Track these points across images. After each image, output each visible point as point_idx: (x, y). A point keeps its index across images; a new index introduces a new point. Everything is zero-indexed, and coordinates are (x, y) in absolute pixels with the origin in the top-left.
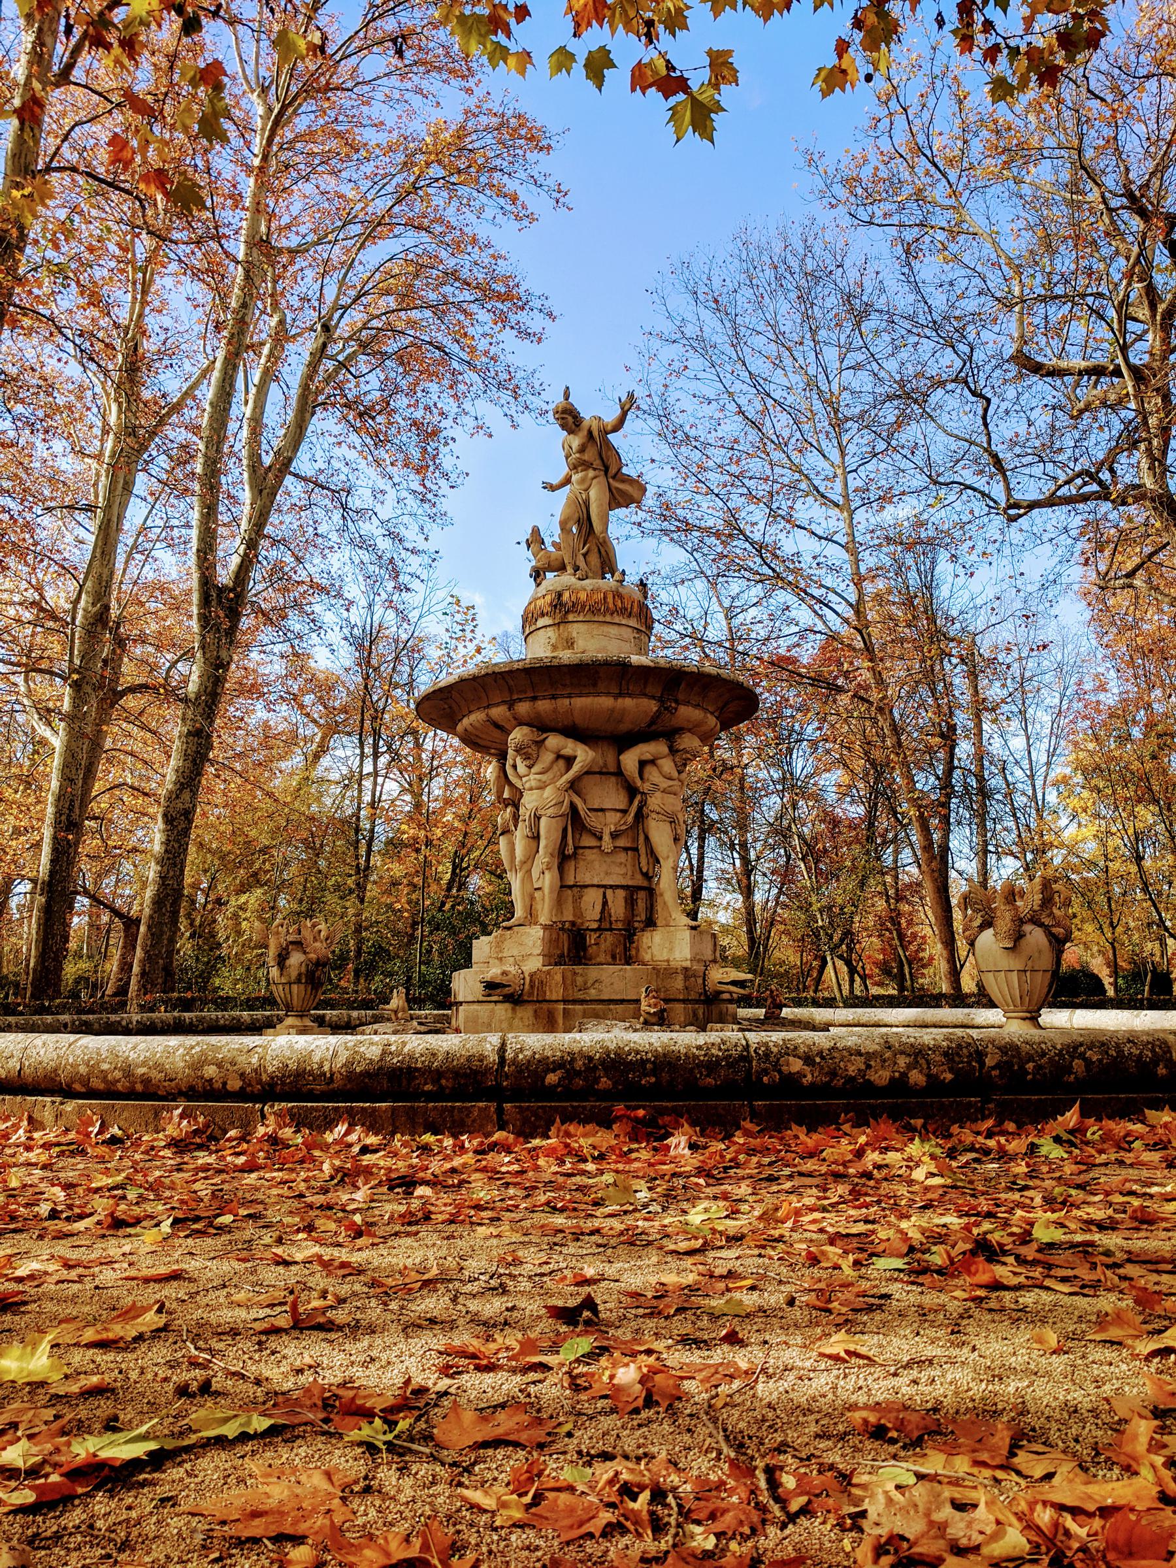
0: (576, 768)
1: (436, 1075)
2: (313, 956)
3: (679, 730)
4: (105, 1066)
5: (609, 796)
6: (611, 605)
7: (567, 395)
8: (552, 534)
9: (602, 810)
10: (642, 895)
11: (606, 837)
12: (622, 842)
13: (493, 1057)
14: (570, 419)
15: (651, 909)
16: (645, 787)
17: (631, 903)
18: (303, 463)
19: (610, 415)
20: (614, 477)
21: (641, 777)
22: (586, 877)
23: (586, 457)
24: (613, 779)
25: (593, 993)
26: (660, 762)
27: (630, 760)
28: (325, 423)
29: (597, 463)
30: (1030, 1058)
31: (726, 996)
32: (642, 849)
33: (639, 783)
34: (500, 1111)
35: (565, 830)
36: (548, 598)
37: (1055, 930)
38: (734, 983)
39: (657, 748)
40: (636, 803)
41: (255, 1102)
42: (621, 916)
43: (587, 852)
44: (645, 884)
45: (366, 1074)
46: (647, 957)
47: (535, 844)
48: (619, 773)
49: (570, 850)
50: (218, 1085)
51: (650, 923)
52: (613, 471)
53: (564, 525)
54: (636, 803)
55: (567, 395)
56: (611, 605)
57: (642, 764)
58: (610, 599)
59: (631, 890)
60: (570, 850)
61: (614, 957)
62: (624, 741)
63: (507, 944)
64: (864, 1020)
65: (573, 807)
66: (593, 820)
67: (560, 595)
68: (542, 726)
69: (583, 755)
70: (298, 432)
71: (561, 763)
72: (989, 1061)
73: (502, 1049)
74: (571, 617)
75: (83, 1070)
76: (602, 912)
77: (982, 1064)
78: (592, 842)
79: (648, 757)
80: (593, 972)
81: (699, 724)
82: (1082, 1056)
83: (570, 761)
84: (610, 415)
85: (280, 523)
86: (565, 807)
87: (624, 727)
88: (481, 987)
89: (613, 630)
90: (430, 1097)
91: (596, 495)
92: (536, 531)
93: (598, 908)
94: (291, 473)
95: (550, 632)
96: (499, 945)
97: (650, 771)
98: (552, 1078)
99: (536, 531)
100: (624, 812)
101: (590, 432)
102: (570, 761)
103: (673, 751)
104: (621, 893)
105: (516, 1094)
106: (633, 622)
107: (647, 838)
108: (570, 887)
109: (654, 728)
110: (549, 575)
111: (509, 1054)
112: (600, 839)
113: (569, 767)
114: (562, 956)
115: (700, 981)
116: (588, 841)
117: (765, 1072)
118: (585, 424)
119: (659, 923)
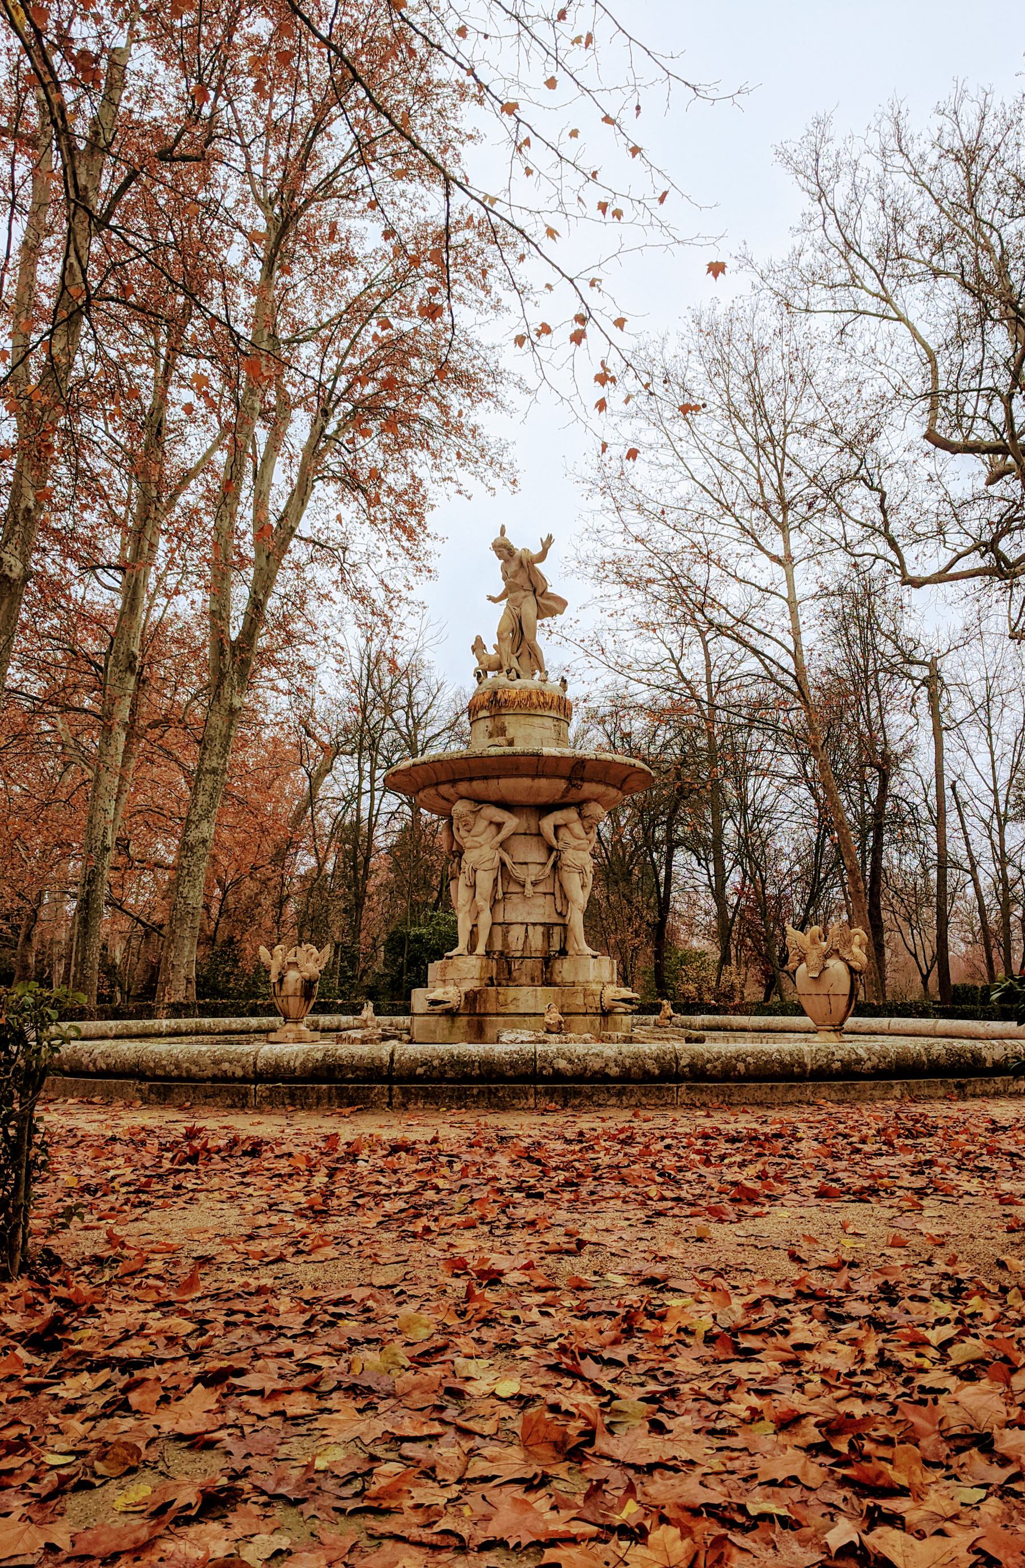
0: (505, 832)
1: (354, 1068)
2: (306, 974)
3: (586, 801)
4: (164, 1062)
5: (532, 853)
6: (535, 700)
7: (503, 532)
8: (491, 641)
9: (526, 863)
10: (557, 930)
11: (529, 886)
12: (541, 888)
13: (387, 1059)
14: (505, 552)
15: (564, 940)
16: (560, 845)
17: (547, 936)
18: (305, 527)
19: (536, 550)
20: (541, 595)
21: (557, 838)
22: (511, 917)
23: (518, 581)
24: (535, 839)
25: (512, 1009)
26: (571, 825)
27: (547, 824)
28: (324, 491)
29: (527, 586)
30: (709, 1061)
31: (620, 1010)
32: (558, 894)
33: (554, 842)
34: (390, 1090)
35: (496, 880)
36: (486, 696)
37: (853, 964)
38: (624, 1000)
39: (571, 814)
40: (553, 857)
41: (251, 1083)
42: (540, 947)
43: (513, 896)
44: (560, 921)
45: (315, 1068)
46: (558, 980)
47: (472, 891)
48: (539, 834)
49: (500, 895)
50: (230, 1074)
51: (563, 952)
52: (540, 591)
53: (499, 635)
54: (553, 857)
55: (503, 532)
56: (535, 700)
57: (557, 828)
58: (534, 697)
59: (548, 927)
60: (500, 895)
61: (533, 979)
62: (545, 809)
63: (450, 969)
64: (773, 1026)
65: (503, 864)
66: (518, 872)
67: (496, 693)
68: (480, 801)
69: (512, 822)
70: (301, 493)
71: (493, 828)
72: (683, 1063)
73: (392, 1054)
74: (503, 711)
75: (152, 1064)
76: (525, 942)
77: (678, 1064)
78: (517, 889)
79: (561, 822)
80: (512, 992)
81: (604, 795)
82: (744, 1060)
83: (499, 826)
84: (536, 550)
85: (285, 582)
86: (496, 863)
87: (542, 799)
88: (427, 1003)
89: (537, 721)
90: (350, 1081)
91: (529, 608)
92: (479, 640)
93: (521, 942)
94: (296, 536)
95: (488, 722)
96: (444, 969)
97: (562, 832)
98: (420, 1071)
99: (479, 640)
100: (544, 864)
101: (521, 563)
102: (499, 826)
103: (582, 817)
104: (540, 929)
105: (400, 1080)
106: (553, 714)
107: (561, 885)
108: (500, 924)
109: (565, 800)
110: (490, 674)
111: (396, 1057)
112: (524, 886)
113: (499, 832)
114: (491, 979)
115: (598, 998)
116: (514, 888)
117: (544, 1068)
118: (517, 554)
119: (571, 952)
